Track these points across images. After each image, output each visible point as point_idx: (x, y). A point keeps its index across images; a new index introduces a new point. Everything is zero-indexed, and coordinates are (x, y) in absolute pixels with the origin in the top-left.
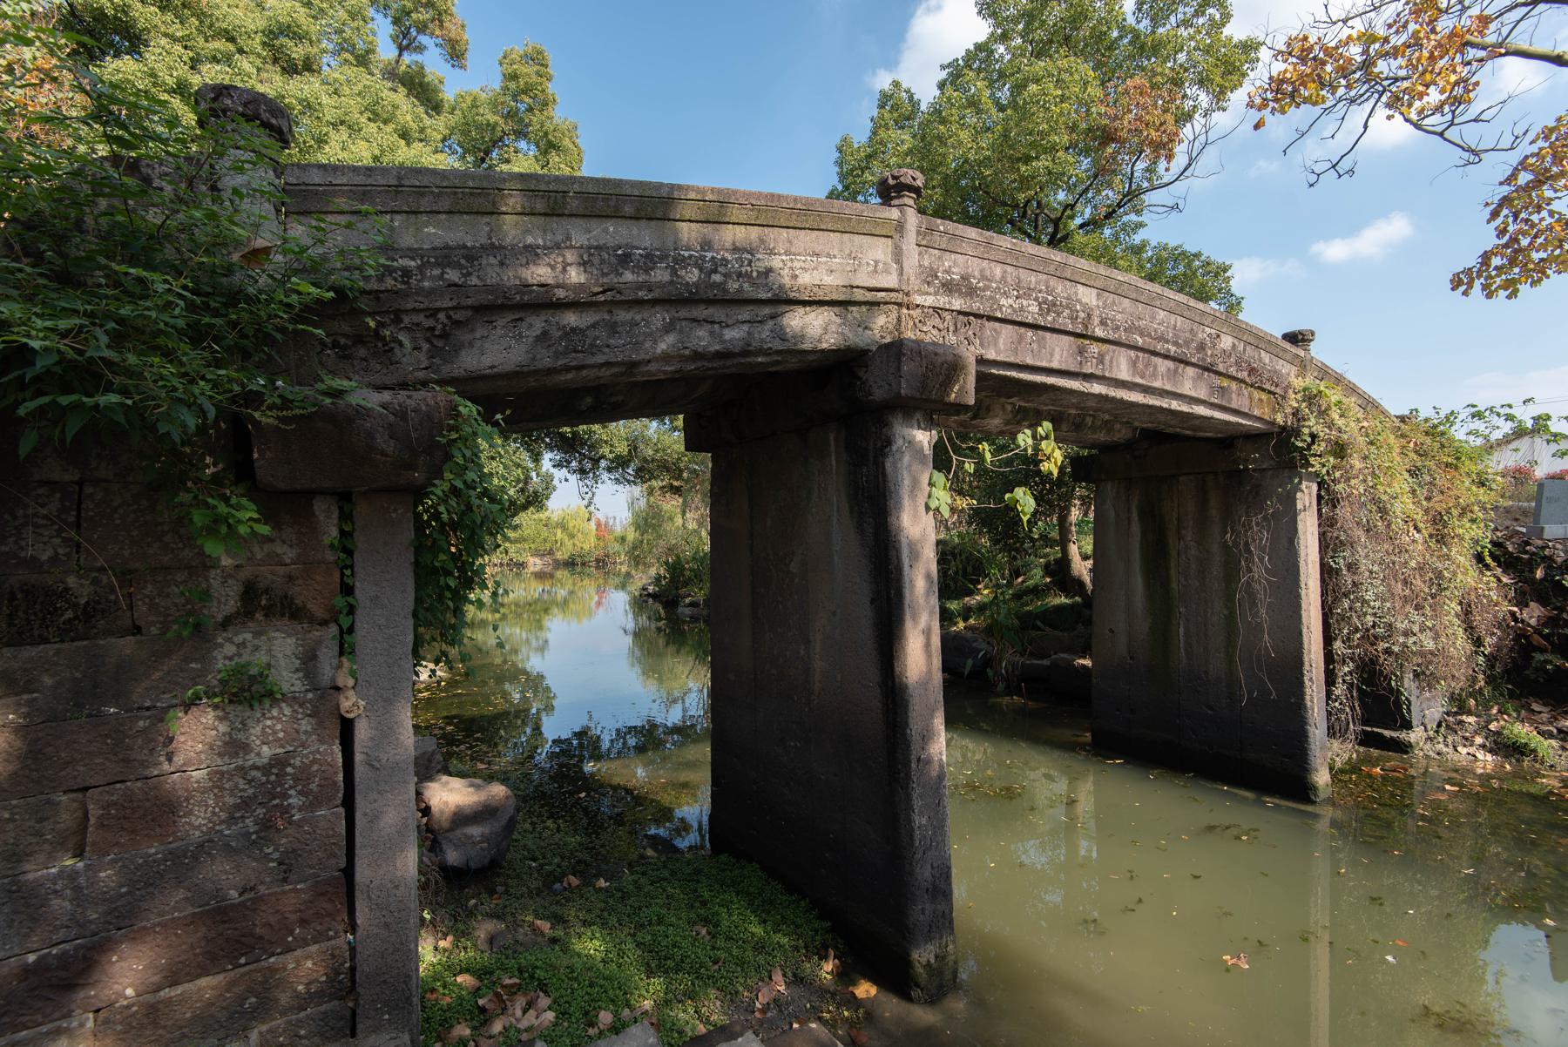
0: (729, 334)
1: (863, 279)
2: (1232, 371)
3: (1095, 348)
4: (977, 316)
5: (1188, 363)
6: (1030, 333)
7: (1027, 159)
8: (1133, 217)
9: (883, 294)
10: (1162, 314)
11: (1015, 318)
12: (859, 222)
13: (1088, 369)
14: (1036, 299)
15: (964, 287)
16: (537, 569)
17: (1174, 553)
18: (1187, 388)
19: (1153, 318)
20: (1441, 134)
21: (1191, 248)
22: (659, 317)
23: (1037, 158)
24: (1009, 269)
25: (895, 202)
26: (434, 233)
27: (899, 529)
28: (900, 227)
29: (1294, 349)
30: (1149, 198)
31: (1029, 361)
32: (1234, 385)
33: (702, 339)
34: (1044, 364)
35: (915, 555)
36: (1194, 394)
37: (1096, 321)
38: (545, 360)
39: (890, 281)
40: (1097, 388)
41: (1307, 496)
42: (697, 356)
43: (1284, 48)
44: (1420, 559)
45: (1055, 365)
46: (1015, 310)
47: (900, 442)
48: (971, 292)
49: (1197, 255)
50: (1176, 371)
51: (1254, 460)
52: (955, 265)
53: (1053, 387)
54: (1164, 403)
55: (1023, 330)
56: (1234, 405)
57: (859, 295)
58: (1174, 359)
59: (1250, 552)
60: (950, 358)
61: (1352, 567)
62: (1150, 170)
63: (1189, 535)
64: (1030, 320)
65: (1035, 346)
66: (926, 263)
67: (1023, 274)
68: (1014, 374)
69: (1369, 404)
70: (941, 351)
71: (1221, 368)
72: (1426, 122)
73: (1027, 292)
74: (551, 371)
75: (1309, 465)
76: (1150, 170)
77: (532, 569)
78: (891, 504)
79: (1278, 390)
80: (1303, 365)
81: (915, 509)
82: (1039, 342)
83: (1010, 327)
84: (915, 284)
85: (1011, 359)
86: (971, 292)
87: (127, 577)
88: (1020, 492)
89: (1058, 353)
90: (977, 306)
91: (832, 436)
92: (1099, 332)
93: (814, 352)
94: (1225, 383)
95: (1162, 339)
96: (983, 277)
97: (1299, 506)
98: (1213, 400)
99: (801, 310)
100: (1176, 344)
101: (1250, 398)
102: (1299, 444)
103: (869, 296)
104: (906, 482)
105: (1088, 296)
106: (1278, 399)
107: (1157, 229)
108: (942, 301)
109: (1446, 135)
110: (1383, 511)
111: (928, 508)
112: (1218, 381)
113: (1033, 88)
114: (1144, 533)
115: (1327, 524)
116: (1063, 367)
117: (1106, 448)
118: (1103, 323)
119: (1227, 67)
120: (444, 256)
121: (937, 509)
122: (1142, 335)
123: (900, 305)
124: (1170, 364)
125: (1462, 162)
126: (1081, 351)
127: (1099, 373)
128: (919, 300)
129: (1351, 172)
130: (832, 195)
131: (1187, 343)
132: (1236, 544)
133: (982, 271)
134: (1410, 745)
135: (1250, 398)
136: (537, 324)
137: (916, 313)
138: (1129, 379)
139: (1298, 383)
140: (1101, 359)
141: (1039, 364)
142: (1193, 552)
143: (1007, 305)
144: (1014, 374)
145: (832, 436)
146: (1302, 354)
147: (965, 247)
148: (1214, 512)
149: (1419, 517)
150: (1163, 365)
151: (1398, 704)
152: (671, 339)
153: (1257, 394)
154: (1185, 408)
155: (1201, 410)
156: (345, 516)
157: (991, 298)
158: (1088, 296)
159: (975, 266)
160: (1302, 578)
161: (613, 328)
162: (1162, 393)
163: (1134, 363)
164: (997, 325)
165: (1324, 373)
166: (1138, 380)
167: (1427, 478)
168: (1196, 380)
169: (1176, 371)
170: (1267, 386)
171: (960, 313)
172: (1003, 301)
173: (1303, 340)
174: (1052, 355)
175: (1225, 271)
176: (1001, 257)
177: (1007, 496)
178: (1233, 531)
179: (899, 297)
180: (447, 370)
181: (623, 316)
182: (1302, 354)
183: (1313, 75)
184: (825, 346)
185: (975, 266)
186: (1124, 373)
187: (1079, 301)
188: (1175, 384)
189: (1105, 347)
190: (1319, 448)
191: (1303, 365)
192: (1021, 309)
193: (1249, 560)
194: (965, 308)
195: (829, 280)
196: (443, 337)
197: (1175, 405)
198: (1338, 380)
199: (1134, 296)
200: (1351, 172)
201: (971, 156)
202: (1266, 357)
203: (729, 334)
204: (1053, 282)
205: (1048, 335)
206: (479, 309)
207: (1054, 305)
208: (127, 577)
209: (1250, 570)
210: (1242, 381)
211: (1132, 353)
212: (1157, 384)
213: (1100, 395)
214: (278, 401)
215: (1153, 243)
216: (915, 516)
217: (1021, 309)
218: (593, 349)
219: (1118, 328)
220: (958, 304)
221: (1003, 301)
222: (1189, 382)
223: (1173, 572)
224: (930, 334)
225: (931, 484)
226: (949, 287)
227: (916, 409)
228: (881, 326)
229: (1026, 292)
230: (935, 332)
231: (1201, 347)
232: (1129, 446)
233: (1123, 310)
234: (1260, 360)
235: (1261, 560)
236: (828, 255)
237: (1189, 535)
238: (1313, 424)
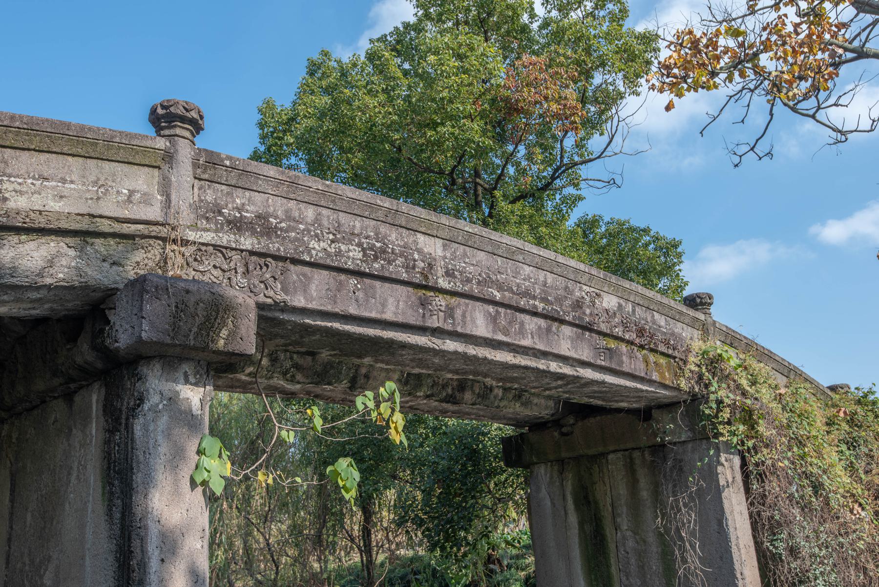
1: (109, 208)
2: (618, 331)
3: (441, 301)
4: (276, 258)
5: (562, 322)
6: (353, 281)
7: (434, 125)
8: (570, 190)
9: (140, 227)
10: (527, 270)
11: (328, 262)
12: (109, 148)
13: (434, 322)
14: (360, 245)
15: (262, 226)
17: (612, 546)
18: (565, 348)
19: (517, 273)
20: (813, 117)
21: (638, 222)
23: (443, 124)
24: (325, 212)
25: (167, 132)
27: (146, 513)
28: (169, 157)
29: (691, 312)
30: (584, 171)
31: (353, 310)
32: (623, 348)
34: (373, 315)
35: (170, 545)
36: (572, 354)
37: (440, 272)
39: (154, 212)
40: (451, 345)
41: (729, 470)
43: (674, 40)
44: (869, 540)
45: (389, 316)
46: (329, 255)
47: (154, 399)
48: (269, 231)
49: (646, 231)
50: (549, 330)
51: (672, 429)
53: (391, 343)
55: (343, 277)
56: (626, 368)
57: (105, 226)
58: (545, 316)
59: (681, 538)
60: (207, 297)
61: (793, 551)
62: (580, 145)
63: (624, 522)
64: (350, 265)
65: (360, 295)
66: (209, 198)
67: (343, 218)
68: (336, 325)
69: (790, 371)
70: (193, 288)
71: (603, 327)
72: (799, 106)
73: (350, 237)
75: (717, 435)
76: (580, 145)
78: (138, 478)
79: (676, 354)
80: (706, 329)
81: (176, 483)
82: (365, 290)
83: (325, 273)
84: (186, 217)
85: (329, 308)
86: (269, 231)
88: (343, 464)
89: (394, 304)
90: (274, 246)
91: (94, 398)
92: (443, 283)
94: (612, 345)
95: (526, 294)
96: (289, 217)
97: (722, 482)
98: (599, 362)
99: (14, 239)
100: (544, 300)
101: (647, 362)
102: (707, 412)
103: (118, 228)
104: (163, 449)
105: (433, 247)
106: (678, 361)
107: (595, 203)
108: (225, 238)
109: (818, 116)
110: (817, 487)
111: (193, 484)
112: (603, 342)
113: (432, 58)
114: (581, 524)
115: (756, 502)
116: (400, 319)
117: (538, 425)
118: (449, 274)
119: (635, 56)
121: (204, 483)
122: (500, 289)
123: (164, 240)
124: (542, 322)
125: (832, 141)
126: (423, 303)
127: (449, 327)
128: (191, 236)
129: (769, 154)
130: (256, 157)
131: (559, 300)
132: (667, 531)
133: (287, 211)
135: (647, 362)
137: (189, 251)
138: (489, 335)
139: (697, 345)
140: (450, 312)
141: (366, 314)
142: (630, 543)
143: (317, 248)
144: (336, 325)
145: (94, 398)
146: (702, 317)
147: (262, 185)
148: (645, 494)
149: (859, 490)
150: (532, 323)
153: (652, 358)
154: (567, 370)
155: (588, 374)
157: (296, 239)
158: (433, 247)
159: (278, 207)
163: (494, 319)
164: (307, 270)
165: (732, 339)
166: (501, 337)
167: (864, 449)
168: (574, 340)
169: (549, 330)
170: (662, 348)
171: (252, 253)
172: (313, 244)
173: (702, 304)
174: (384, 305)
175: (676, 246)
176: (313, 198)
177: (329, 469)
178: (663, 515)
179: (164, 231)
182: (702, 317)
183: (695, 65)
184: (48, 281)
187: (420, 251)
188: (549, 343)
189: (454, 301)
190: (726, 414)
191: (706, 329)
192: (339, 253)
193: (682, 549)
194: (257, 247)
195: (55, 206)
197: (554, 366)
198: (748, 346)
199: (489, 249)
200: (769, 154)
201: (379, 120)
202: (661, 320)
204: (384, 229)
205: (378, 284)
207: (384, 251)
209: (684, 561)
210: (630, 343)
211: (491, 309)
212: (526, 342)
213: (456, 353)
215: (607, 219)
216: (176, 492)
217: (339, 253)
219: (469, 281)
220: (248, 242)
221: (313, 244)
222: (565, 342)
223: (614, 570)
224: (209, 271)
225: (200, 452)
226: (237, 225)
227: (182, 359)
228: (141, 261)
229: (340, 235)
230: (217, 273)
231: (578, 305)
232: (555, 423)
233: (475, 263)
234: (654, 322)
235: (693, 547)
236: (64, 181)
237: (624, 522)
238: (720, 392)
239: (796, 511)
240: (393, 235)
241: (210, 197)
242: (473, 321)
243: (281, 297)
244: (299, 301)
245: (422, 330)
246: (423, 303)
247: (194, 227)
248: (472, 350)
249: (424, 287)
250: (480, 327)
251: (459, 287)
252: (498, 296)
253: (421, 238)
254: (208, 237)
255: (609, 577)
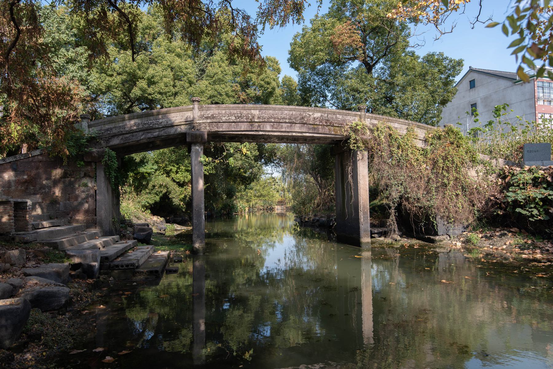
0: (154, 134)
3: (257, 124)
15: (213, 117)
16: (279, 211)
18: (297, 129)
22: (141, 133)
26: (107, 127)
33: (149, 135)
37: (256, 118)
38: (122, 142)
40: (261, 133)
42: (149, 138)
45: (242, 129)
52: (210, 113)
54: (290, 134)
67: (231, 111)
73: (231, 115)
74: (123, 143)
77: (276, 212)
87: (73, 172)
93: (173, 135)
95: (284, 118)
96: (219, 114)
108: (204, 121)
120: (107, 130)
124: (289, 124)
134: (435, 241)
136: (121, 137)
140: (259, 126)
151: (433, 226)
152: (144, 136)
154: (300, 135)
155: (307, 134)
156: (96, 165)
159: (216, 112)
160: (359, 180)
161: (133, 136)
162: (288, 132)
163: (273, 126)
180: (108, 145)
181: (134, 134)
185: (216, 112)
186: (268, 129)
189: (260, 124)
196: (108, 141)
197: (294, 134)
203: (154, 134)
206: (112, 136)
208: (73, 172)
214: (427, 78)
218: (130, 139)
220: (209, 121)
226: (207, 118)
239: (366, 355)
240: (245, 112)
241: (202, 113)
242: (266, 127)
243: (216, 129)
244: (221, 130)
245: (272, 131)
246: (252, 125)
247: (199, 120)
248: (267, 133)
249: (251, 122)
250: (268, 128)
251: (261, 120)
252: (273, 121)
253: (252, 111)
254: (201, 121)
255: (206, 208)
